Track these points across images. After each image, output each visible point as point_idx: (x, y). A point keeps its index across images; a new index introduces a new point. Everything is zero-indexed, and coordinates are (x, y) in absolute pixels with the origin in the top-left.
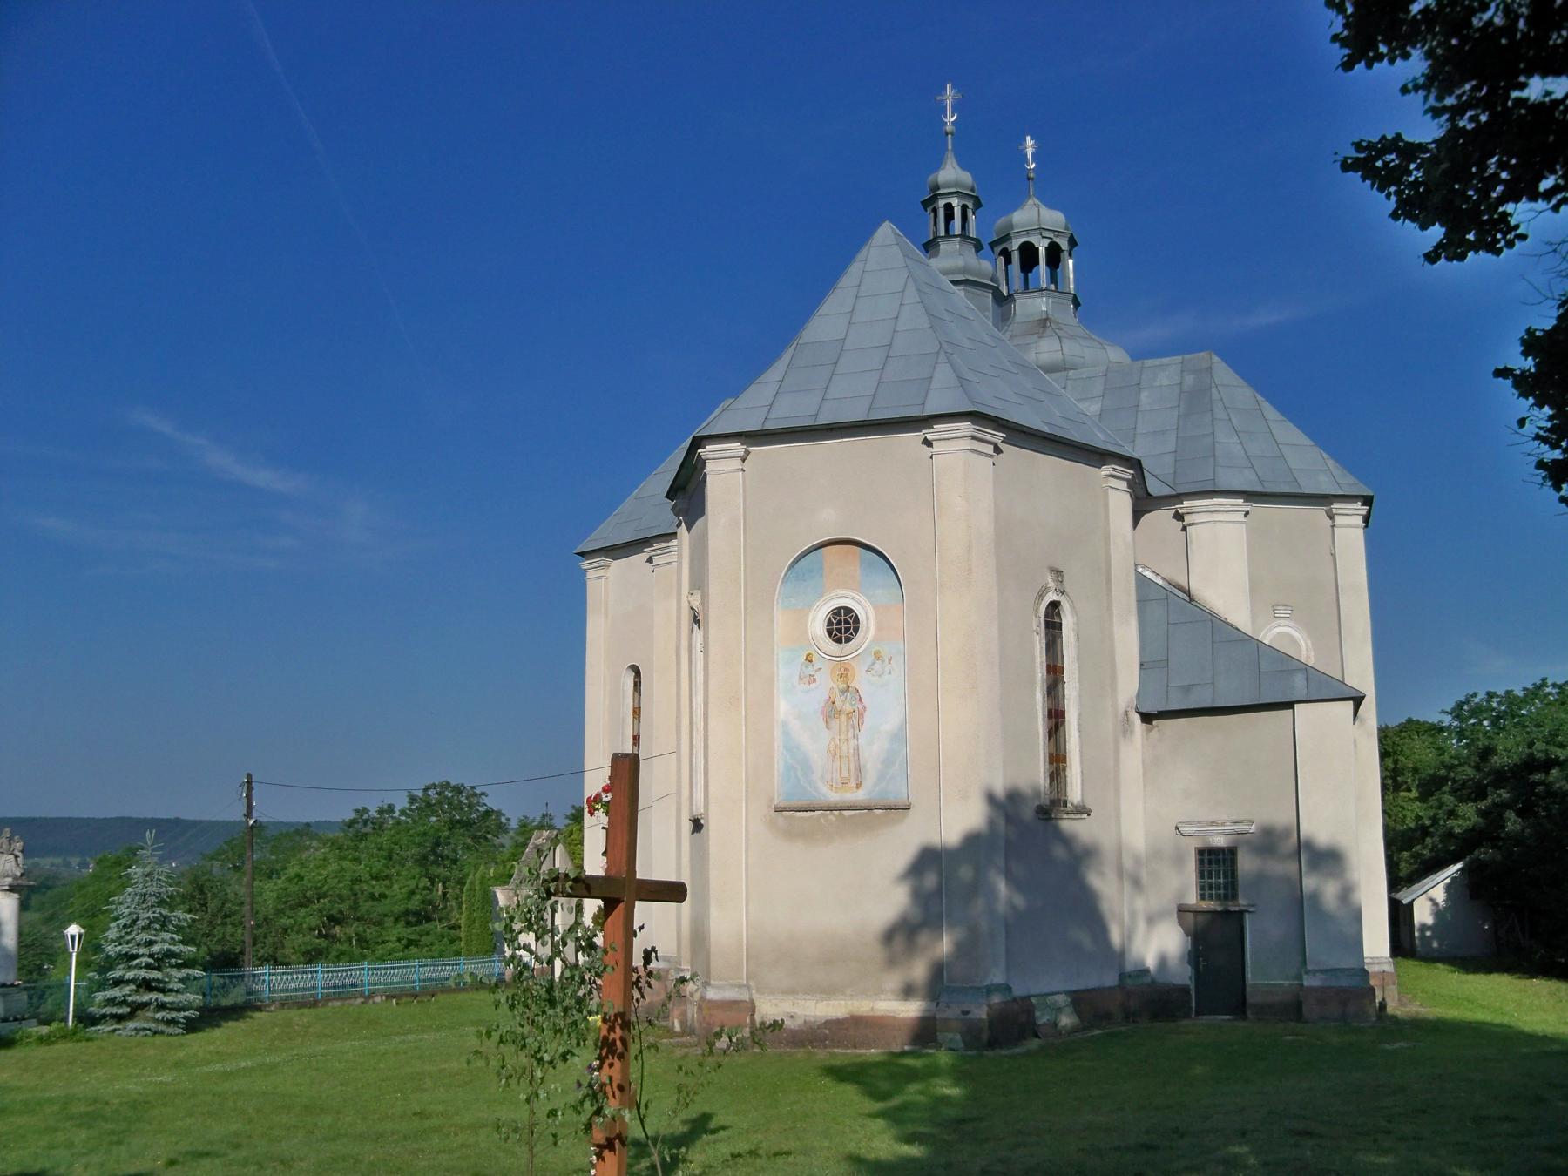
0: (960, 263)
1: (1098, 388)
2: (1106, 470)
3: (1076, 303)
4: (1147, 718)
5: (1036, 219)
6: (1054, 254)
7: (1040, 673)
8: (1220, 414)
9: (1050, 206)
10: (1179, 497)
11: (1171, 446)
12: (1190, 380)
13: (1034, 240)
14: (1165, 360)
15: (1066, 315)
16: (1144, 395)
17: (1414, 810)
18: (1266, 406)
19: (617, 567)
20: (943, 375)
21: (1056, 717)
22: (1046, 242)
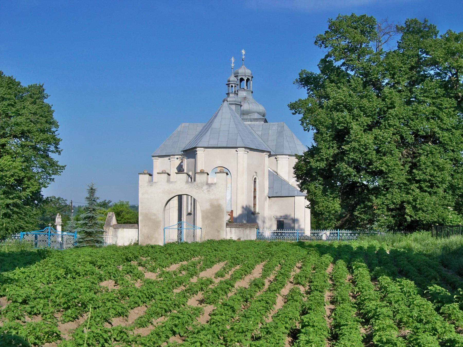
0: (234, 99)
1: (261, 129)
2: (265, 153)
3: (252, 92)
4: (269, 197)
5: (245, 71)
6: (248, 80)
7: (253, 190)
8: (285, 137)
9: (248, 68)
10: (276, 155)
11: (275, 144)
12: (279, 128)
13: (243, 77)
14: (274, 123)
15: (250, 97)
16: (270, 131)
17: (158, 247)
18: (294, 135)
19: (161, 159)
20: (239, 138)
21: (255, 197)
22: (246, 78)
